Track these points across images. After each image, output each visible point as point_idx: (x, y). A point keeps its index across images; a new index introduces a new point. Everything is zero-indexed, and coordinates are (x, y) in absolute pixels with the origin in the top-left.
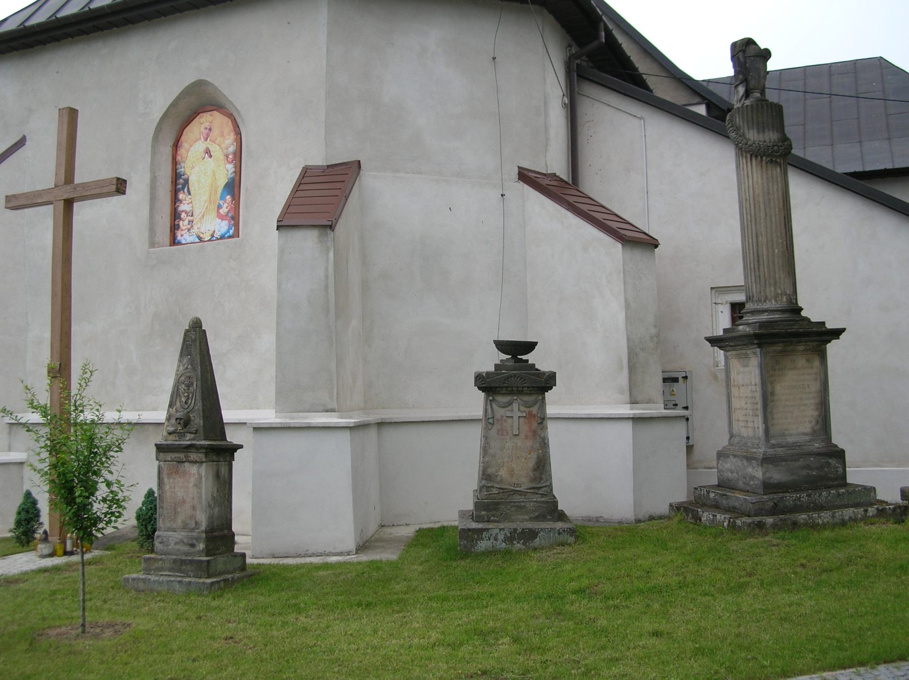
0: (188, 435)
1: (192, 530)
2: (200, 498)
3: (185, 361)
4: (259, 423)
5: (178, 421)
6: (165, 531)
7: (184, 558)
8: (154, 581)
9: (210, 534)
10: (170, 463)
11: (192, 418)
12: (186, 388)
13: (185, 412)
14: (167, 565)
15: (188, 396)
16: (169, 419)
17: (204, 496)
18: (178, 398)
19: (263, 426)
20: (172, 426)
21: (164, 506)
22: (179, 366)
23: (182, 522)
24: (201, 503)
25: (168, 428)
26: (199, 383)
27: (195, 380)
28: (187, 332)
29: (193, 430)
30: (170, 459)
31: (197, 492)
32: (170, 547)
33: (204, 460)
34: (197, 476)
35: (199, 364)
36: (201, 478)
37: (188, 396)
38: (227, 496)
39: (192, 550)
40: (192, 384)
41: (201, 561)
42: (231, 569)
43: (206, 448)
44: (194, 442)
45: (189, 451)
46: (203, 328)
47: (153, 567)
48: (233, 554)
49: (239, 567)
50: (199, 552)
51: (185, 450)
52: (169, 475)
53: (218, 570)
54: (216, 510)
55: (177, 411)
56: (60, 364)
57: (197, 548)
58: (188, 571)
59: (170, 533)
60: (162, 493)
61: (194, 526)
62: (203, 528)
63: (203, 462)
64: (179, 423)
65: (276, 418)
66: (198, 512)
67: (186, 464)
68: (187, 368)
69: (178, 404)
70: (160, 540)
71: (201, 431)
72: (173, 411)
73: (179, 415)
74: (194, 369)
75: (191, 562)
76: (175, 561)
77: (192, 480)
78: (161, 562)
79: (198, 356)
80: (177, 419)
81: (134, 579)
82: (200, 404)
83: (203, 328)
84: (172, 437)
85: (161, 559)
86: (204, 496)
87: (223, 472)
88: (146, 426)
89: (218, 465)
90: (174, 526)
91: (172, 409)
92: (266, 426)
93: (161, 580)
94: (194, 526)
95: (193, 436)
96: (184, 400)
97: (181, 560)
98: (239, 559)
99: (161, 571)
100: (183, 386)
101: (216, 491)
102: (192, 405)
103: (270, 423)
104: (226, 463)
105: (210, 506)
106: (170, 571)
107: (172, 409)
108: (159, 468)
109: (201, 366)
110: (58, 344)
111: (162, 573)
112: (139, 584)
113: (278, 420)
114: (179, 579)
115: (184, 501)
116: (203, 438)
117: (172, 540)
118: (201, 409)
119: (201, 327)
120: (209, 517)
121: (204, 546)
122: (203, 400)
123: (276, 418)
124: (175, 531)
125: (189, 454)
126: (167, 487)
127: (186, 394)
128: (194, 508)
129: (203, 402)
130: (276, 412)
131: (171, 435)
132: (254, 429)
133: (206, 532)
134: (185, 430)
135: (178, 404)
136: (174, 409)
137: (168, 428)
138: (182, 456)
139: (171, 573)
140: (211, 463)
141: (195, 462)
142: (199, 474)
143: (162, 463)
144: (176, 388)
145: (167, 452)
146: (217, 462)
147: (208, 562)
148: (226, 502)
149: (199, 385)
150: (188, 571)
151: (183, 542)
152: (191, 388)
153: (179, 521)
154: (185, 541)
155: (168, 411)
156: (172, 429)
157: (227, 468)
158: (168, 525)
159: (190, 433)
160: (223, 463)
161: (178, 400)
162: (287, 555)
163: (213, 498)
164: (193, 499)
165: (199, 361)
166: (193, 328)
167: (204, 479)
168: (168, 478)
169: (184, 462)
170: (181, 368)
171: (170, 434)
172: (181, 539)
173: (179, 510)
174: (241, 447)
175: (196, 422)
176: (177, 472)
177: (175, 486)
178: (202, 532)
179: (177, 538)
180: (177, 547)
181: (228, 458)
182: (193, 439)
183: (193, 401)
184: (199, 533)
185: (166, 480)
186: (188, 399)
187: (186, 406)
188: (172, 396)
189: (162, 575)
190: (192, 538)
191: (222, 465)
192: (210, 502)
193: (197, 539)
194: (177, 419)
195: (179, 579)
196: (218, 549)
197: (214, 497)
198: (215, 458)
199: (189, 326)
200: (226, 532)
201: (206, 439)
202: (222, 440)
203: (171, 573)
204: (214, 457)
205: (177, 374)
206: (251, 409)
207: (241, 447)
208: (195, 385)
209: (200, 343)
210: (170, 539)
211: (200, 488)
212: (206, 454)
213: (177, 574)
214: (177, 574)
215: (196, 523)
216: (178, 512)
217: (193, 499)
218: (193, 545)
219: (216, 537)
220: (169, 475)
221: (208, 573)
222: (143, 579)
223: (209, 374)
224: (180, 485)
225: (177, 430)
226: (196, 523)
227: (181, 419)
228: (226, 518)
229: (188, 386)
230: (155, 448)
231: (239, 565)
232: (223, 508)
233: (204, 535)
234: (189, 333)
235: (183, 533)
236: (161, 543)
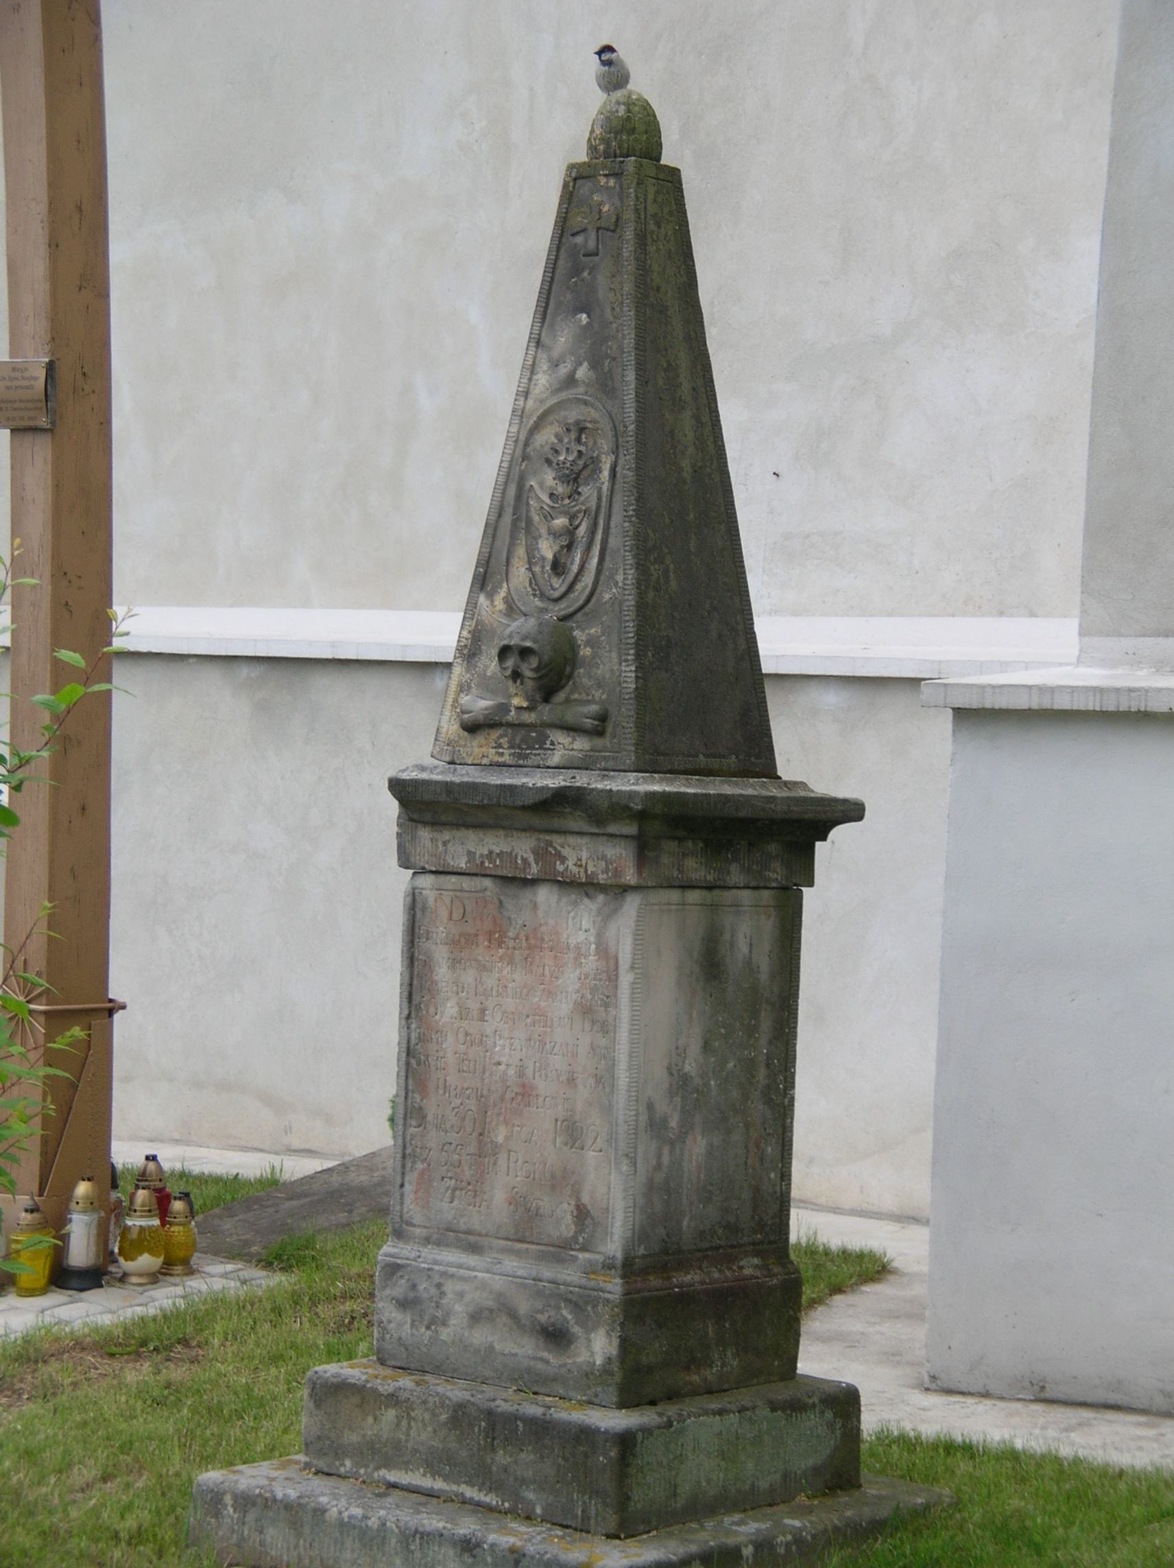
0: (561, 738)
1: (560, 1251)
2: (604, 1079)
3: (563, 339)
4: (982, 687)
5: (510, 663)
6: (427, 1241)
7: (506, 1401)
8: (343, 1526)
9: (654, 1282)
10: (466, 882)
11: (586, 652)
12: (560, 489)
13: (552, 616)
14: (422, 1435)
15: (571, 532)
16: (470, 650)
17: (623, 1078)
18: (522, 538)
19: (1002, 702)
20: (487, 686)
21: (431, 1111)
22: (533, 370)
23: (517, 1201)
24: (607, 1110)
25: (465, 699)
26: (627, 460)
27: (605, 444)
28: (577, 177)
29: (585, 712)
30: (462, 864)
31: (593, 1048)
32: (445, 1334)
33: (630, 877)
34: (591, 962)
35: (630, 358)
36: (612, 977)
37: (571, 532)
38: (761, 1075)
39: (553, 1360)
40: (592, 464)
41: (586, 1434)
42: (763, 1484)
43: (642, 816)
44: (582, 780)
45: (557, 823)
46: (664, 161)
47: (352, 1438)
48: (783, 1392)
49: (817, 1470)
50: (588, 1374)
51: (536, 821)
52: (461, 944)
53: (685, 1489)
54: (697, 1146)
55: (511, 609)
56: (50, 367)
57: (582, 1357)
58: (523, 1482)
59: (451, 1256)
60: (422, 1039)
61: (566, 1227)
62: (613, 1245)
63: (625, 889)
64: (516, 675)
65: (1079, 662)
66: (591, 1155)
67: (544, 895)
68: (571, 381)
69: (520, 573)
70: (400, 1288)
71: (625, 719)
72: (492, 608)
73: (518, 630)
74: (605, 385)
75: (541, 1429)
76: (460, 1416)
77: (570, 980)
78: (391, 1414)
79: (628, 319)
80: (504, 652)
81: (245, 1501)
82: (624, 576)
83: (664, 161)
84: (482, 747)
85: (393, 1399)
86: (623, 1078)
87: (743, 947)
88: (324, 686)
89: (714, 907)
90: (475, 1220)
91: (490, 596)
92: (1022, 702)
93: (373, 1522)
94: (566, 1227)
95: (581, 744)
96: (547, 549)
97: (490, 1414)
98: (815, 1423)
99: (388, 1465)
100: (549, 477)
101: (695, 1048)
102: (588, 579)
103: (1041, 689)
104: (766, 894)
105: (656, 1126)
106: (432, 1465)
107: (490, 596)
108: (415, 907)
109: (640, 367)
110: (38, 267)
111: (393, 1476)
112: (271, 1533)
113: (1093, 676)
114: (468, 1526)
115: (526, 1092)
116: (630, 760)
117: (460, 1295)
118: (631, 601)
119: (652, 150)
120: (651, 1188)
121: (614, 1350)
122: (645, 553)
123: (1079, 662)
124: (475, 1249)
125: (557, 840)
126: (450, 1010)
127: (560, 522)
128: (572, 1132)
129: (642, 568)
130: (1083, 632)
131: (480, 738)
132: (962, 714)
133: (629, 1268)
134: (545, 712)
135: (520, 573)
136: (499, 604)
137: (465, 699)
138: (522, 847)
139: (439, 1484)
140: (675, 895)
141: (584, 887)
142: (603, 951)
143: (426, 881)
144: (512, 490)
145: (457, 825)
146: (710, 888)
147: (626, 1441)
148: (758, 1109)
149: (627, 473)
150: (523, 1482)
151: (513, 1315)
152: (587, 491)
153: (499, 1196)
154: (523, 1307)
155: (471, 607)
156: (484, 704)
157: (769, 925)
158: (445, 1209)
159: (572, 729)
160: (746, 895)
161: (521, 551)
162: (1113, 1398)
163: (680, 1083)
164: (571, 1081)
165: (629, 341)
166: (607, 155)
167: (626, 979)
168: (455, 963)
169: (534, 882)
170: (542, 380)
171: (472, 728)
172: (500, 1296)
173: (500, 1136)
174: (853, 811)
175: (601, 671)
176: (497, 937)
177: (483, 1011)
178: (608, 1266)
179: (483, 1286)
180: (480, 1336)
181: (776, 873)
182: (584, 765)
183: (594, 561)
184: (590, 1270)
185: (442, 973)
186: (569, 547)
187: (559, 585)
188: (491, 531)
189: (394, 1486)
190: (558, 1295)
191: (736, 905)
192: (662, 1107)
193: (582, 1303)
194: (504, 652)
195: (468, 1526)
196: (692, 1363)
197: (685, 1079)
198: (695, 868)
199: (592, 149)
200: (750, 1266)
201: (648, 767)
202: (745, 773)
203: (439, 1484)
204: (690, 863)
205: (519, 414)
206: (1001, 614)
207: (853, 811)
208: (606, 474)
209: (642, 240)
210: (450, 1287)
211: (606, 1028)
212: (644, 848)
213: (470, 1492)
214: (470, 1492)
215: (582, 1214)
216: (496, 1149)
217: (571, 1081)
218: (556, 1337)
219: (685, 1299)
220: (461, 944)
221: (623, 1502)
222: (288, 1506)
223: (687, 414)
224: (509, 1003)
225: (504, 708)
226: (582, 1214)
227: (524, 653)
228: (756, 1191)
229: (574, 478)
230: (392, 807)
231: (810, 1462)
232: (737, 1137)
233: (614, 1287)
234: (585, 188)
235: (511, 1264)
236: (404, 1304)
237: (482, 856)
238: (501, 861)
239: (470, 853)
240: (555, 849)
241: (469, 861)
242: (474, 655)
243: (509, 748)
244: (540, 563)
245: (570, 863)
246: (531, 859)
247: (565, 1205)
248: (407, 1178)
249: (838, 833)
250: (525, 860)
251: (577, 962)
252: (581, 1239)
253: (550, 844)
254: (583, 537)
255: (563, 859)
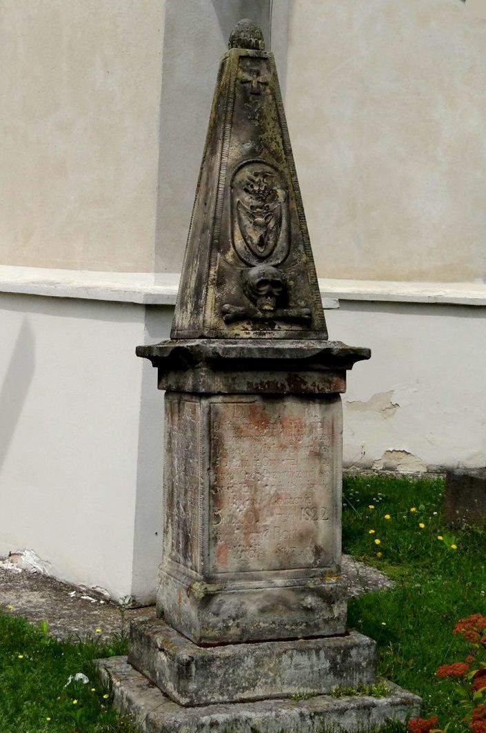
30: (245, 388)
185: (230, 441)
207: (361, 355)
237: (256, 384)
238: (268, 386)
239: (249, 383)
240: (300, 378)
241: (248, 387)
242: (221, 284)
243: (252, 330)
244: (249, 239)
245: (309, 385)
246: (286, 384)
247: (308, 548)
248: (211, 550)
249: (358, 365)
250: (282, 385)
251: (311, 432)
252: (318, 562)
253: (297, 376)
254: (273, 228)
255: (305, 383)
